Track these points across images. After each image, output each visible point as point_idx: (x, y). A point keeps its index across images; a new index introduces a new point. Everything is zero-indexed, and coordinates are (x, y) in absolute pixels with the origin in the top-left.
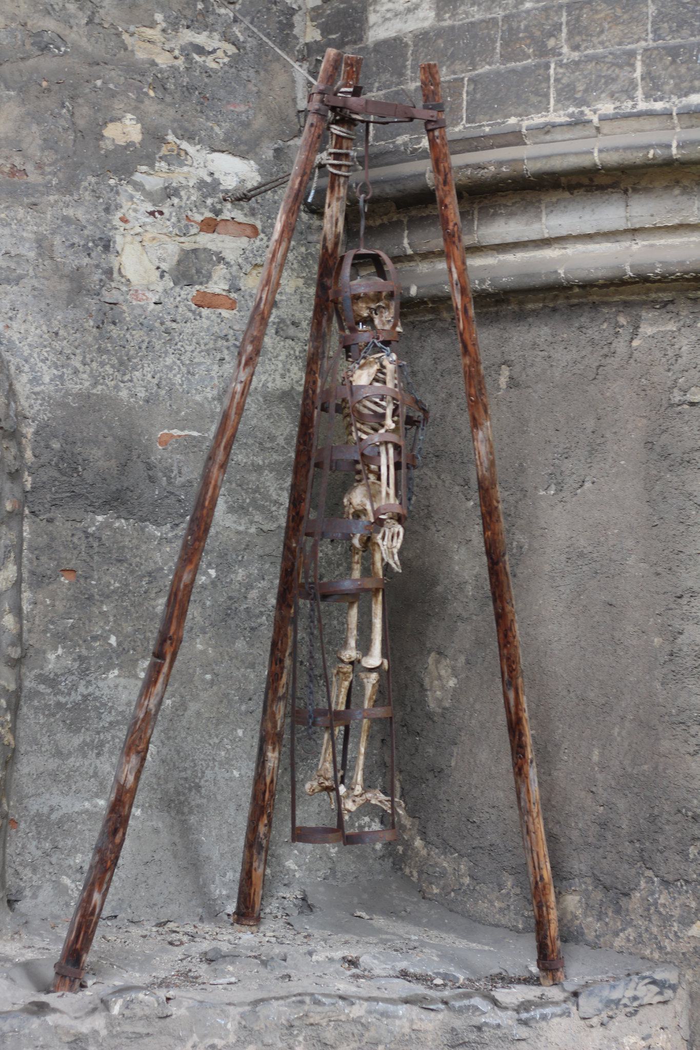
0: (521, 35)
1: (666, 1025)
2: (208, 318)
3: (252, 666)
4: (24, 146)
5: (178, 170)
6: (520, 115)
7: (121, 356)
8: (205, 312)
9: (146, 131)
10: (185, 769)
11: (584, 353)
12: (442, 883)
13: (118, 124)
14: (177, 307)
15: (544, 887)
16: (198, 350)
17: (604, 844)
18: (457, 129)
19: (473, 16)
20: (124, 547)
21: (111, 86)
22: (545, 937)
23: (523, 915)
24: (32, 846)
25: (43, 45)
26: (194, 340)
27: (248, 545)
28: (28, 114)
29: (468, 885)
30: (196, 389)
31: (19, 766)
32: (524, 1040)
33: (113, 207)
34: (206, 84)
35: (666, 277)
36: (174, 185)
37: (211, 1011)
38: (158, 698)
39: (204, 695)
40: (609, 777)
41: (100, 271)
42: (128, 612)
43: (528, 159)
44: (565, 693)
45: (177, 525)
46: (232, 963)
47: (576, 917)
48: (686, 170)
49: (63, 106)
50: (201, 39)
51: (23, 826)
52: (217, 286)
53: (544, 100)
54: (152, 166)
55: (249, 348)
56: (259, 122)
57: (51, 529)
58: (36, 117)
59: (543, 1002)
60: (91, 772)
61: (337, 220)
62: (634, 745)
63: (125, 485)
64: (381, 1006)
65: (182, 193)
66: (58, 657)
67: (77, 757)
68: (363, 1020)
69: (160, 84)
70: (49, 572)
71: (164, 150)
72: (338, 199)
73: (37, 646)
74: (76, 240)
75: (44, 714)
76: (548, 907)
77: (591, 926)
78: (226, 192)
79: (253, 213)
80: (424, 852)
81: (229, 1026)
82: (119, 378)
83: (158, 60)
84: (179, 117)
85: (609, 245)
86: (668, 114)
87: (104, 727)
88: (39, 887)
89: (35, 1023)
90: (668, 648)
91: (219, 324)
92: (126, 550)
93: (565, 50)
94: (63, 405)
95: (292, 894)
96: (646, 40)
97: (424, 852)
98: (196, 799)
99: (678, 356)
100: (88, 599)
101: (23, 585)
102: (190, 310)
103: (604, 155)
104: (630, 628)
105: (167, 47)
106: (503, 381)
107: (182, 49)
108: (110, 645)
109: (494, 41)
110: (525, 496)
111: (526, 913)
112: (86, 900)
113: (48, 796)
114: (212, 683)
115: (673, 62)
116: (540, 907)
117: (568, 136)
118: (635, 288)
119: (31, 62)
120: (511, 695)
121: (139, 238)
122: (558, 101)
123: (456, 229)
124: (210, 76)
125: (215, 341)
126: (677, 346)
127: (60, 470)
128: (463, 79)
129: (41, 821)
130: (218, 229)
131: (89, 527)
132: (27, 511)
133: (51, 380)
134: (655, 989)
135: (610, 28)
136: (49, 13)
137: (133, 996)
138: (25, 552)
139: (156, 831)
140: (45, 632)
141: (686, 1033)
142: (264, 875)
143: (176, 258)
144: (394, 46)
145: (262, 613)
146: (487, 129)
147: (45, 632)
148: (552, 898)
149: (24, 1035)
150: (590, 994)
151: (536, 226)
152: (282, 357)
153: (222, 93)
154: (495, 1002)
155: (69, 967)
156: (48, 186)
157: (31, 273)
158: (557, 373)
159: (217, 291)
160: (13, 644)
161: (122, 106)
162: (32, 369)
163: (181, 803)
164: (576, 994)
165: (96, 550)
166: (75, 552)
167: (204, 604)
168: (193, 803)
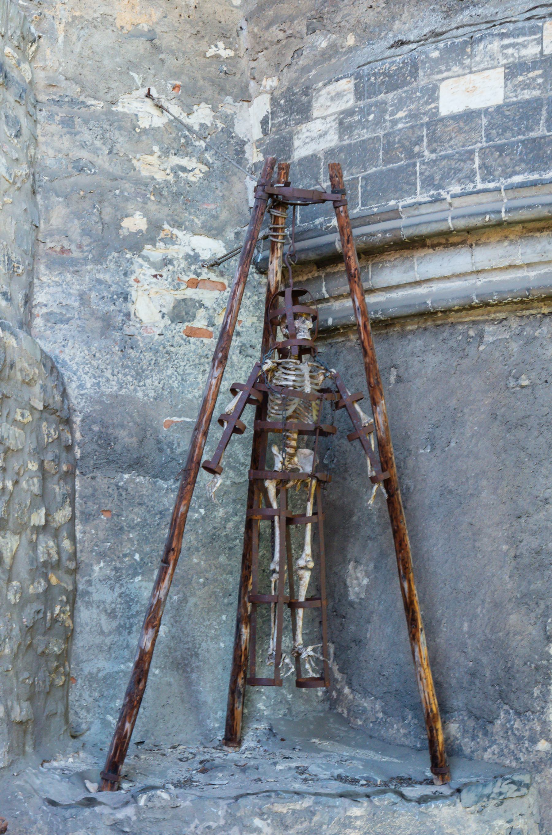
0: (396, 146)
1: (523, 813)
2: (194, 344)
3: (231, 573)
4: (69, 234)
5: (171, 247)
6: (398, 199)
7: (137, 370)
8: (192, 340)
9: (149, 222)
10: (187, 643)
11: (446, 357)
12: (364, 717)
13: (131, 218)
14: (173, 337)
15: (434, 717)
16: (188, 365)
17: (474, 688)
18: (355, 211)
19: (363, 136)
20: (143, 495)
21: (126, 194)
22: (436, 751)
23: (420, 738)
24: (86, 695)
25: (80, 168)
26: (186, 358)
27: (225, 493)
28: (72, 213)
29: (382, 719)
30: (188, 391)
31: (76, 641)
33: (129, 272)
34: (188, 191)
35: (500, 302)
36: (169, 257)
37: (207, 803)
38: (166, 590)
40: (475, 642)
41: (122, 314)
42: (147, 538)
43: (404, 227)
44: (443, 585)
46: (221, 771)
47: (457, 739)
48: (513, 229)
49: (94, 207)
50: (184, 162)
51: (80, 681)
52: (200, 323)
53: (413, 187)
54: (154, 245)
55: (220, 355)
56: (224, 215)
57: (94, 483)
58: (78, 215)
59: (436, 797)
60: (125, 645)
61: (277, 272)
62: (492, 620)
63: (143, 454)
65: (175, 263)
66: (101, 568)
67: (115, 635)
69: (158, 192)
70: (93, 512)
71: (162, 235)
72: (277, 258)
73: (87, 561)
74: (105, 294)
78: (204, 261)
79: (222, 274)
80: (351, 697)
81: (220, 813)
82: (136, 384)
83: (156, 177)
84: (171, 213)
85: (461, 283)
86: (498, 190)
87: (132, 615)
88: (92, 723)
89: (87, 812)
91: (202, 348)
92: (145, 497)
93: (426, 153)
96: (481, 142)
97: (351, 697)
98: (195, 663)
100: (120, 529)
101: (76, 521)
102: (182, 339)
105: (162, 168)
106: (393, 379)
107: (172, 169)
108: (135, 560)
109: (378, 152)
110: (410, 454)
111: (422, 737)
112: (121, 728)
113: (96, 661)
114: (204, 585)
115: (501, 155)
116: (431, 731)
117: (430, 210)
118: (479, 311)
119: (72, 179)
120: (406, 585)
122: (422, 188)
123: (356, 272)
124: (190, 186)
125: (200, 359)
126: (510, 349)
127: (99, 445)
128: (358, 178)
129: (92, 677)
130: (199, 285)
131: (119, 482)
132: (78, 472)
133: (92, 386)
134: (514, 787)
135: (456, 136)
136: (83, 147)
138: (77, 499)
139: (169, 684)
140: (92, 551)
141: (537, 818)
142: (243, 713)
143: (172, 305)
144: (312, 160)
145: (236, 538)
147: (92, 551)
148: (439, 725)
151: (411, 273)
152: (244, 369)
154: (402, 796)
155: (110, 773)
156: (85, 259)
157: (76, 316)
160: (70, 559)
161: (133, 206)
162: (79, 379)
163: (186, 665)
164: (459, 791)
165: (124, 497)
166: (111, 499)
167: (197, 532)
168: (194, 665)
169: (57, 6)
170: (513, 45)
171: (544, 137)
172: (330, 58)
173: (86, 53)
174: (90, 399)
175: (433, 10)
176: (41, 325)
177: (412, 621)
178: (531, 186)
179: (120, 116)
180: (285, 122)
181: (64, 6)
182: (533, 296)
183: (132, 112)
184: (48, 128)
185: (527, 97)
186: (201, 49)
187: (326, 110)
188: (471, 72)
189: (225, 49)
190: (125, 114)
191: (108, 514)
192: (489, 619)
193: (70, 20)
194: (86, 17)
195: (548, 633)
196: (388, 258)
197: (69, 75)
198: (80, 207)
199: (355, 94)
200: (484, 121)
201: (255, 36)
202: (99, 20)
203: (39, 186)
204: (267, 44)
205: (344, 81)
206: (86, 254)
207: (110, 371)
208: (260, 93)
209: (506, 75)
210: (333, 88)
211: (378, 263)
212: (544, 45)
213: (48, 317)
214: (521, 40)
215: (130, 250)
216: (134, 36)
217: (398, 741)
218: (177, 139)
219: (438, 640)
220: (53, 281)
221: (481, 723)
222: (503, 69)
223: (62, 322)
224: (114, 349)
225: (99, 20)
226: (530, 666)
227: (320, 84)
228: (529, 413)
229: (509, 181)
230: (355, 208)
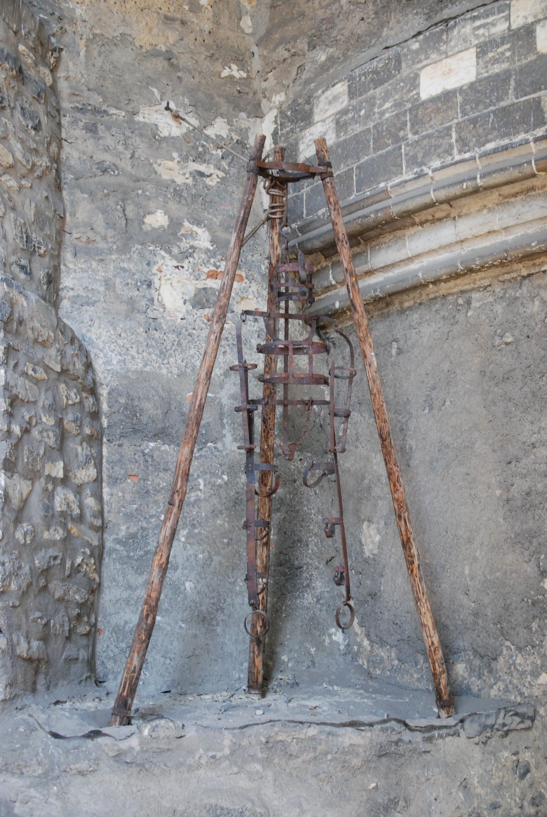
4: (95, 227)
6: (386, 181)
9: (171, 219)
11: (439, 326)
14: (195, 321)
21: (148, 193)
25: (103, 169)
31: (103, 595)
32: (429, 752)
33: (152, 263)
34: (207, 194)
40: (476, 583)
43: (393, 205)
44: (444, 533)
45: (202, 449)
47: (465, 679)
50: (202, 168)
64: (328, 728)
70: (120, 477)
71: (183, 231)
73: (114, 521)
74: (129, 281)
75: (119, 563)
77: (475, 684)
83: (176, 179)
86: (473, 159)
89: (90, 743)
93: (410, 136)
94: (125, 377)
96: (457, 118)
98: (221, 616)
100: (146, 492)
102: (204, 323)
106: (394, 351)
107: (191, 173)
109: (368, 142)
114: (228, 544)
119: (97, 179)
121: (170, 282)
127: (125, 415)
129: (119, 630)
132: (105, 440)
133: (118, 362)
134: (517, 719)
135: (435, 116)
138: (105, 464)
140: (119, 512)
146: (368, 193)
147: (119, 512)
151: (403, 251)
153: (217, 199)
157: (102, 299)
158: (425, 340)
161: (155, 205)
162: (105, 356)
163: (212, 619)
164: (462, 721)
166: (137, 465)
168: (219, 619)
169: (78, 23)
170: (483, 26)
171: (513, 105)
172: (328, 70)
173: (107, 67)
174: (115, 374)
175: (417, 14)
176: (68, 306)
178: (503, 150)
179: (141, 125)
180: (292, 131)
181: (85, 24)
182: (511, 257)
183: (153, 122)
185: (497, 71)
186: (216, 70)
187: (325, 113)
188: (447, 57)
189: (238, 70)
190: (145, 123)
191: (136, 480)
192: (487, 561)
193: (91, 37)
195: (542, 569)
196: (384, 240)
197: (91, 86)
198: (105, 204)
199: (349, 95)
200: (460, 99)
201: (264, 58)
202: (118, 39)
203: (65, 184)
204: (275, 64)
205: (339, 85)
206: (111, 245)
207: (135, 350)
208: (271, 109)
209: (477, 53)
210: (329, 94)
211: (375, 246)
212: (512, 20)
213: (74, 300)
214: (490, 20)
215: (152, 243)
216: (152, 55)
217: (412, 686)
218: (195, 147)
220: (79, 268)
221: (486, 661)
222: (475, 49)
223: (88, 304)
224: (138, 331)
225: (118, 39)
226: (528, 602)
227: (320, 92)
229: (483, 149)
230: (352, 194)
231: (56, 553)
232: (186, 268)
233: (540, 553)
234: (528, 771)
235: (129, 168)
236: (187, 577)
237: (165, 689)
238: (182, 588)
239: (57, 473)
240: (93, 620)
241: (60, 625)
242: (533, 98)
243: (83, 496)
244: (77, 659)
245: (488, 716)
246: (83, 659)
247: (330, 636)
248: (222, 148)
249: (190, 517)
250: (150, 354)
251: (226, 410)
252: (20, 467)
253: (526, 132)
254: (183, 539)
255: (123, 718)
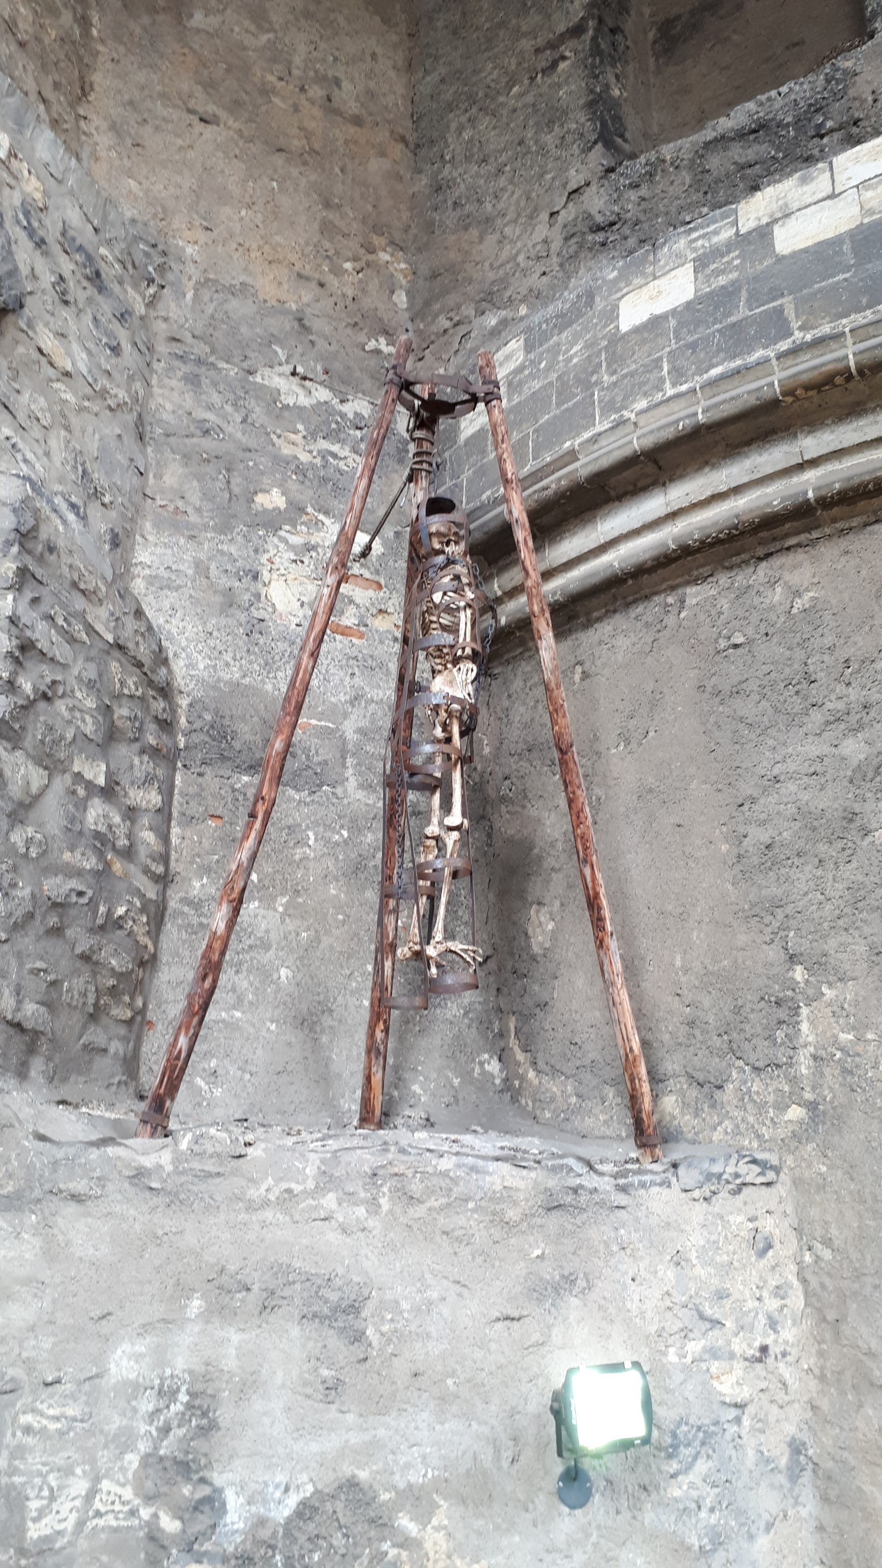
1: (772, 1209)
2: (341, 642)
9: (289, 502)
12: (552, 1107)
13: (267, 495)
15: (635, 1060)
28: (191, 473)
32: (623, 1208)
39: (336, 932)
44: (646, 910)
47: (674, 1118)
50: (335, 448)
58: (199, 478)
64: (470, 1160)
65: (320, 550)
66: (203, 885)
68: (451, 1174)
74: (229, 568)
76: (640, 1080)
77: (686, 1122)
81: (308, 1171)
85: (654, 535)
90: (735, 851)
94: (215, 688)
95: (417, 1114)
98: (327, 1021)
99: (720, 613)
103: (641, 441)
104: (698, 842)
105: (307, 448)
106: (577, 677)
107: (319, 452)
109: (550, 397)
114: (344, 922)
115: (694, 352)
119: (195, 440)
120: (587, 871)
122: (601, 416)
132: (179, 765)
134: (756, 1169)
137: (204, 1130)
138: (176, 797)
140: (192, 863)
149: (80, 1165)
150: (689, 1166)
151: (594, 536)
158: (620, 657)
159: (349, 624)
162: (188, 657)
164: (675, 1166)
168: (325, 1024)
170: (703, 236)
171: (746, 319)
173: (219, 316)
174: (200, 681)
175: (613, 258)
177: (598, 922)
184: (166, 381)
185: (723, 283)
188: (655, 278)
190: (263, 386)
191: (219, 822)
193: (202, 280)
194: (222, 282)
197: (197, 333)
200: (673, 323)
204: (433, 337)
206: (206, 520)
212: (740, 225)
213: (151, 580)
214: (712, 228)
217: (597, 1133)
219: (643, 985)
223: (169, 588)
224: (236, 631)
228: (746, 676)
231: (81, 888)
232: (306, 562)
233: (788, 929)
234: (770, 1246)
235: (239, 435)
236: (283, 961)
237: (237, 1116)
238: (275, 976)
239: (95, 776)
240: (139, 1003)
241: (80, 993)
242: (774, 307)
243: (137, 828)
244: (105, 1050)
245: (713, 1160)
246: (115, 1054)
247: (481, 1064)
248: (361, 429)
249: (292, 880)
250: (251, 662)
251: (350, 747)
252: (28, 743)
253: (765, 347)
254: (281, 909)
255: (156, 1128)
